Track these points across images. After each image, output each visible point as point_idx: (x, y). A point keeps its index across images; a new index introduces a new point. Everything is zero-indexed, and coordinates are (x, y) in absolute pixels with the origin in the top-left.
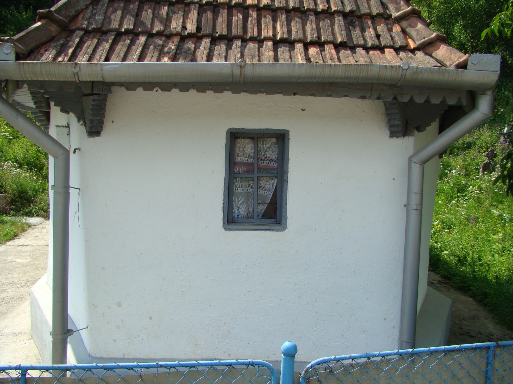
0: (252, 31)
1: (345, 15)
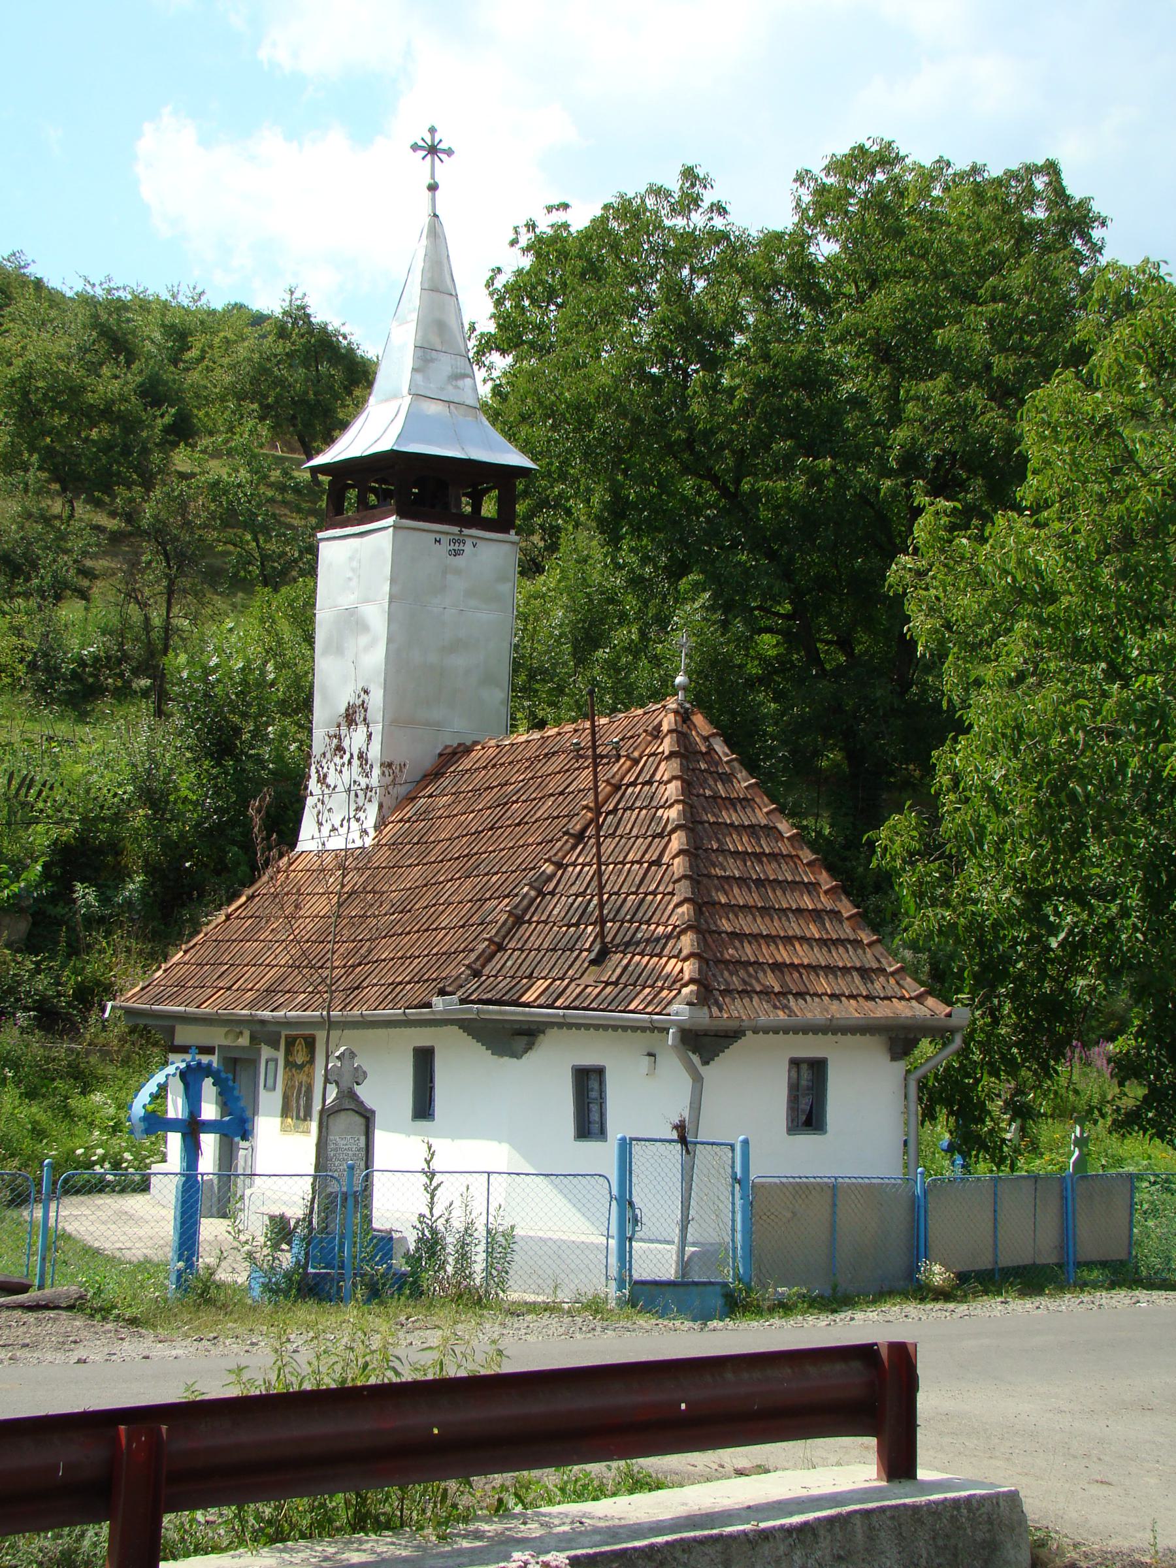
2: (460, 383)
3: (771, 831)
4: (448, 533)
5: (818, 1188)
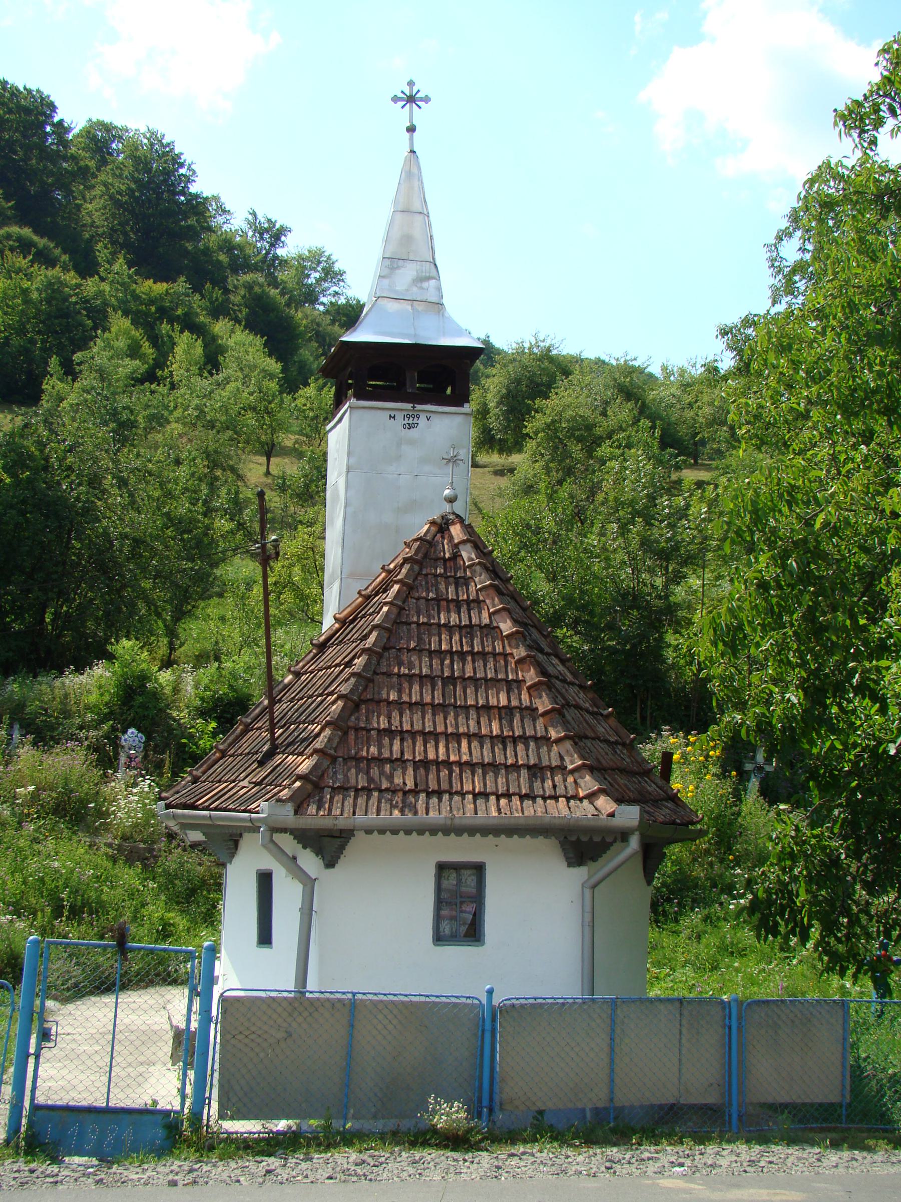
0: (456, 786)
1: (529, 767)
2: (425, 285)
3: (490, 630)
4: (402, 410)
5: (327, 1005)
